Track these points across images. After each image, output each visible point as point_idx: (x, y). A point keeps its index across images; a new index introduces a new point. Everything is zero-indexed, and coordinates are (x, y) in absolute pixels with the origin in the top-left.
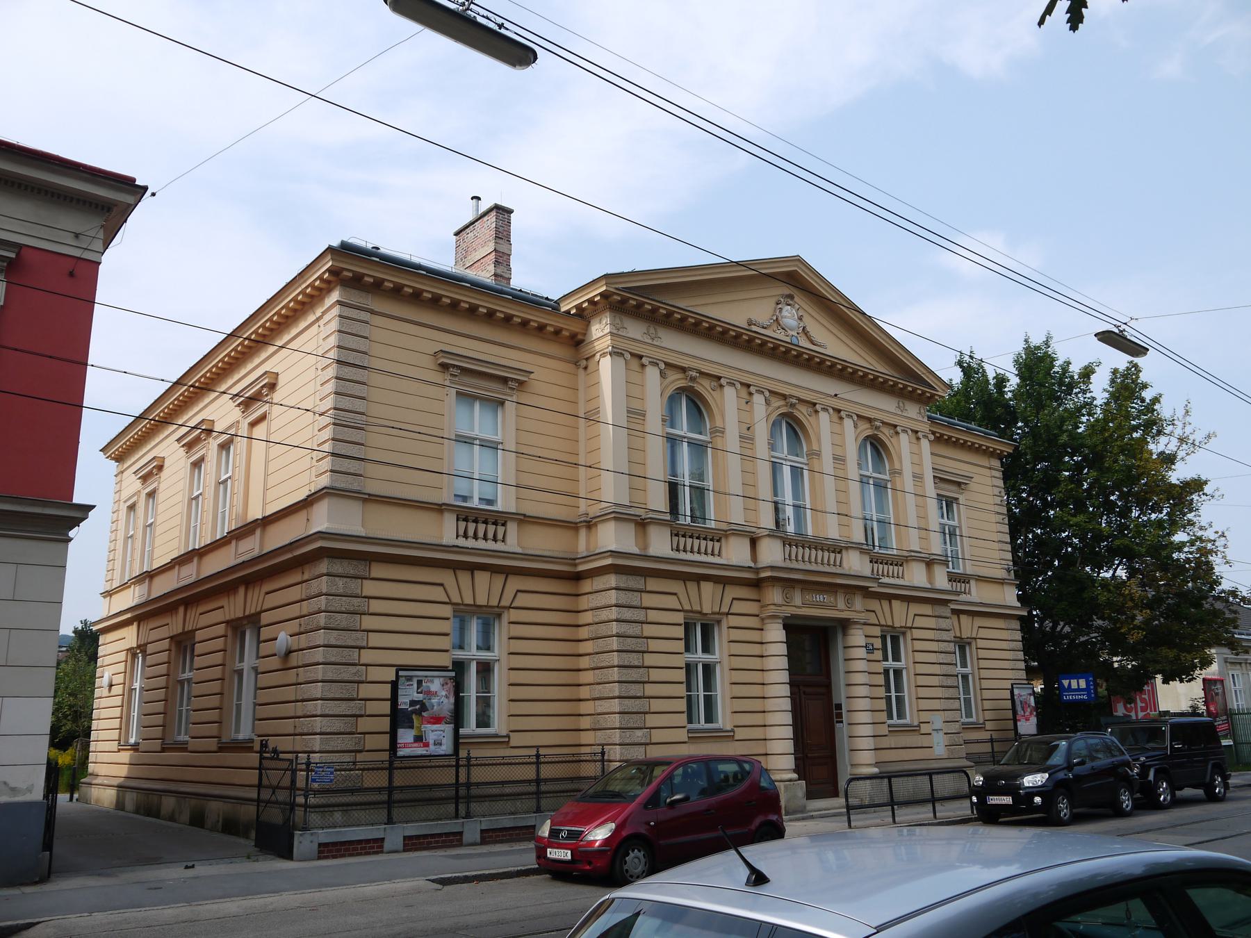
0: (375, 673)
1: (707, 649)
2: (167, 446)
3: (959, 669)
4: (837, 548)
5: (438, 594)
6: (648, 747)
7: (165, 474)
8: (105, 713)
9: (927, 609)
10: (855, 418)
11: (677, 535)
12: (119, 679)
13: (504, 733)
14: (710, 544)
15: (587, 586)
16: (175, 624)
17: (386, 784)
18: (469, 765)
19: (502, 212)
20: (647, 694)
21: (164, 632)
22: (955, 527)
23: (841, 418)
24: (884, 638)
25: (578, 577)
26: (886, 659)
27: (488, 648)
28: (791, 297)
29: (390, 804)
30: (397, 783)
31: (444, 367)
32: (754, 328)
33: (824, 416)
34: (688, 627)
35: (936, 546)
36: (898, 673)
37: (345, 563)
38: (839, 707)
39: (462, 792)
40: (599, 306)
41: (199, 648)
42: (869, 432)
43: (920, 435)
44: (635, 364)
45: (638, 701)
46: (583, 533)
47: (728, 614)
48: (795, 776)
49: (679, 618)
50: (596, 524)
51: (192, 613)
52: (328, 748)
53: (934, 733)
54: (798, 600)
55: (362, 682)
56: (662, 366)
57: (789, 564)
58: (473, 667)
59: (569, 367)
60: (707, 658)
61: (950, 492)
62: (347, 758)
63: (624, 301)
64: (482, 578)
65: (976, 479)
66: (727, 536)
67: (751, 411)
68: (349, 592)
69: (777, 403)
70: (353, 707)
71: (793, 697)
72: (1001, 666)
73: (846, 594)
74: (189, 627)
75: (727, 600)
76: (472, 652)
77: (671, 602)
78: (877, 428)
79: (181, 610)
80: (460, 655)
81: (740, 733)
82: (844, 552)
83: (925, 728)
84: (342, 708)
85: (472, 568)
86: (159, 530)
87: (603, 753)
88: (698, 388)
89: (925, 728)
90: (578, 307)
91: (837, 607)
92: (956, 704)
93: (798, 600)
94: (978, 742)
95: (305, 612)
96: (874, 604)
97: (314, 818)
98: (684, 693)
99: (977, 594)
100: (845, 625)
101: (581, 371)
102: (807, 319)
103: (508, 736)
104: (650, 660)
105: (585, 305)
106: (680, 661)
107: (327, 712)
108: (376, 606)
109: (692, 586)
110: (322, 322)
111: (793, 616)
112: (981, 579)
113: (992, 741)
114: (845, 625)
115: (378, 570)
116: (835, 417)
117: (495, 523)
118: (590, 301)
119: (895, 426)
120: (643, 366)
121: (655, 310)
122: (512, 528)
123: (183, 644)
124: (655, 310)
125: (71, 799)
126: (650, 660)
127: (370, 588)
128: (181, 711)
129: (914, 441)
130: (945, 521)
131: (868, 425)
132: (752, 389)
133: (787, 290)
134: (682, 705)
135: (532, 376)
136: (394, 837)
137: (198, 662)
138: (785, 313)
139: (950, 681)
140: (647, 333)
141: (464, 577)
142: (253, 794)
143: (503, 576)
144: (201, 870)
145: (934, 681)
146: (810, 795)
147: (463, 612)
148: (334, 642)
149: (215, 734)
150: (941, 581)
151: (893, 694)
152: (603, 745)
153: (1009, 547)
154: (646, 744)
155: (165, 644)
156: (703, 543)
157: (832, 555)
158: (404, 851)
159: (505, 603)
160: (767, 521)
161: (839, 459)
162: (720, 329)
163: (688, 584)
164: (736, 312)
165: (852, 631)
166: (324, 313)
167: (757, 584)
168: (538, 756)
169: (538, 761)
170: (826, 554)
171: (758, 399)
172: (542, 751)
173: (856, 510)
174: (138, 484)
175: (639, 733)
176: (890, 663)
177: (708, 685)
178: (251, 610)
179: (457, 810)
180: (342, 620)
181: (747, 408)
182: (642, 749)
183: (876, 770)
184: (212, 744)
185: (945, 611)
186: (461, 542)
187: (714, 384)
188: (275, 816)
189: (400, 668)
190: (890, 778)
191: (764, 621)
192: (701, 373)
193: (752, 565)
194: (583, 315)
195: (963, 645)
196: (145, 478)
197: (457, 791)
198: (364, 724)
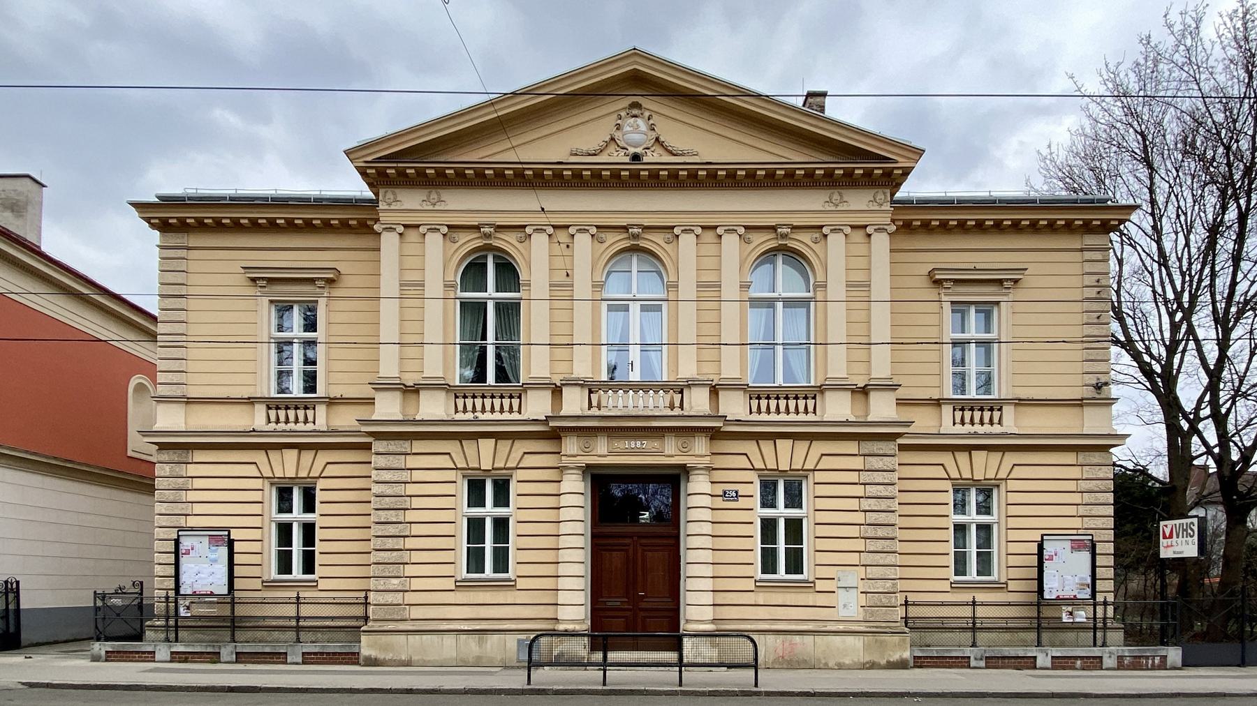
13: (1003, 581)
28: (636, 105)
31: (938, 283)
37: (171, 452)
44: (858, 236)
45: (395, 553)
53: (841, 592)
58: (974, 528)
66: (525, 391)
75: (516, 455)
87: (366, 598)
91: (668, 453)
115: (199, 456)
122: (1008, 411)
127: (192, 470)
159: (1002, 475)
167: (555, 435)
168: (298, 598)
189: (181, 529)
192: (794, 228)
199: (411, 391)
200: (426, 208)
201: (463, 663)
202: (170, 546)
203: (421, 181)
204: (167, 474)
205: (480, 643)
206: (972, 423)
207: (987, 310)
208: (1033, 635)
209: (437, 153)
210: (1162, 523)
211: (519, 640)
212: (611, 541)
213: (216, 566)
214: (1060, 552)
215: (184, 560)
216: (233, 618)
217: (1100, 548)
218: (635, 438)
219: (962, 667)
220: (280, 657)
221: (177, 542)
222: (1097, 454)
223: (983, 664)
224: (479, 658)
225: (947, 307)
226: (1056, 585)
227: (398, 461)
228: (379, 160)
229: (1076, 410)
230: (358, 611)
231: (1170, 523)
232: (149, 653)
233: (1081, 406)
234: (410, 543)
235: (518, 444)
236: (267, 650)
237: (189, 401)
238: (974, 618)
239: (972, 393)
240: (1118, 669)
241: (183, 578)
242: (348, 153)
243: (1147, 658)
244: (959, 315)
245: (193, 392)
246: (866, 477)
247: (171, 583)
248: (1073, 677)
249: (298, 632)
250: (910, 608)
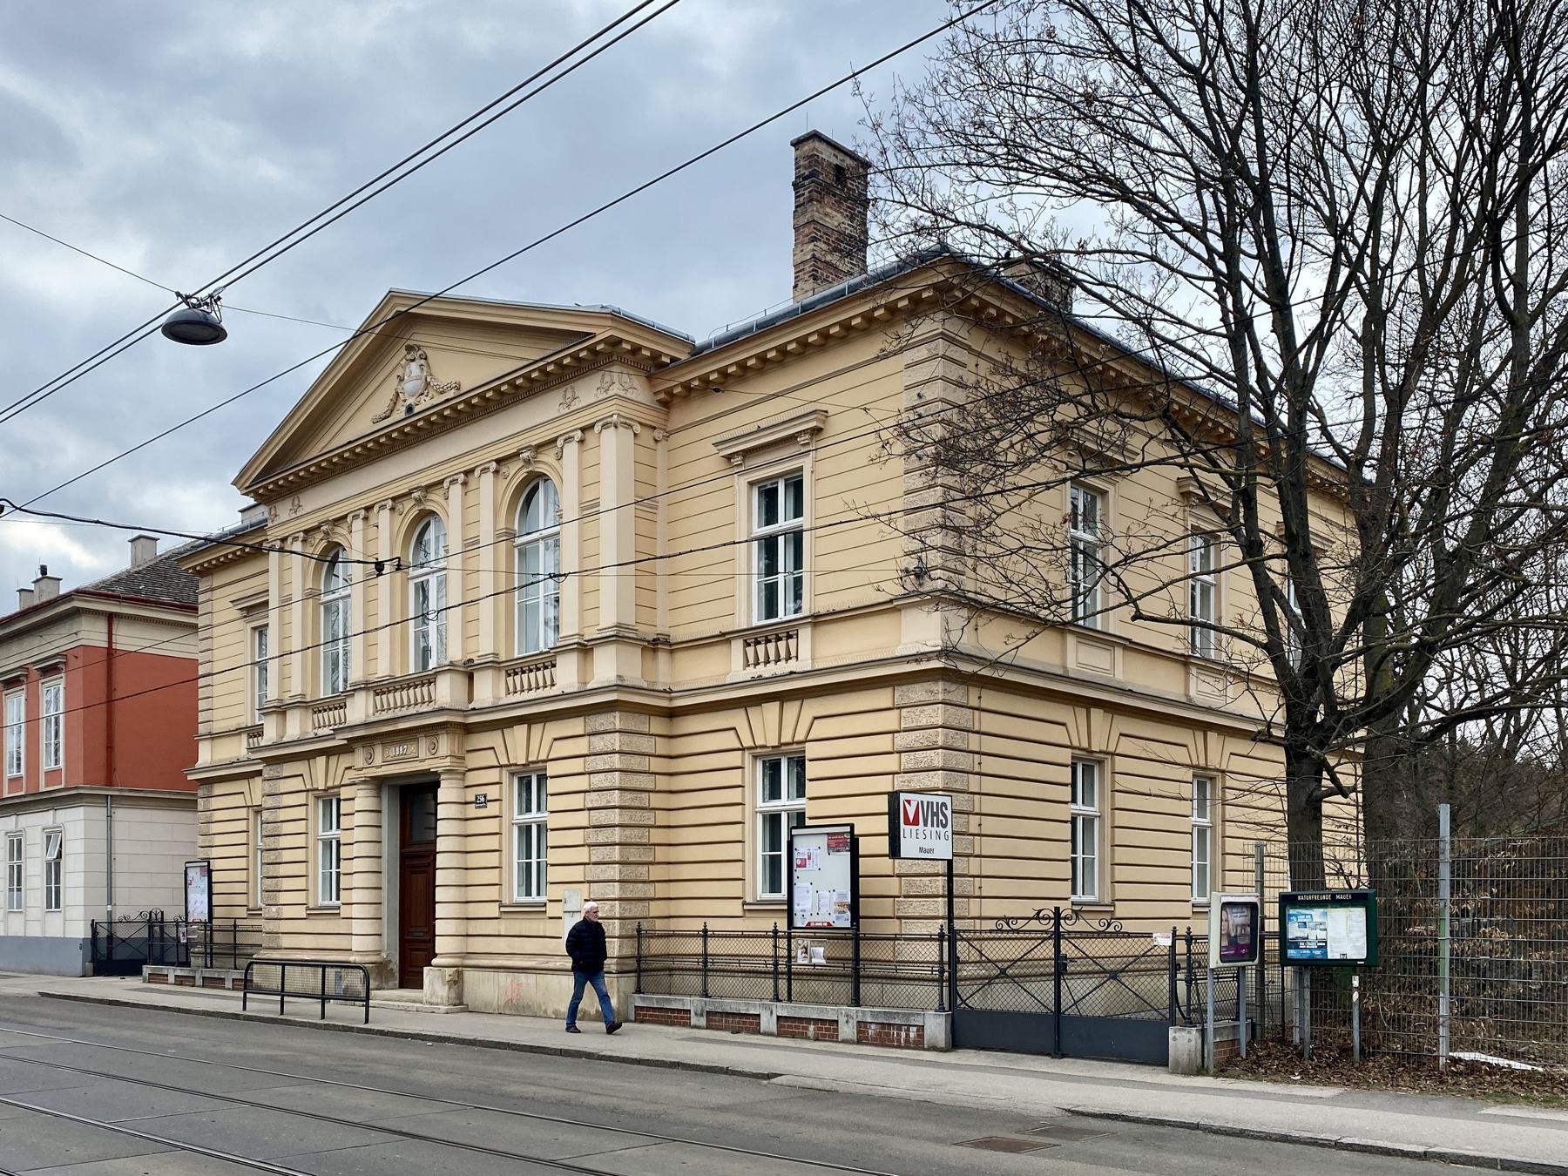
3: (1195, 819)
9: (576, 726)
26: (1074, 801)
49: (1065, 756)
106: (1065, 812)
115: (219, 789)
122: (805, 634)
168: (639, 931)
176: (1079, 808)
184: (301, 912)
208: (845, 988)
209: (294, 458)
212: (416, 862)
216: (235, 946)
217: (865, 846)
219: (679, 1024)
222: (918, 687)
223: (703, 1021)
226: (808, 906)
229: (721, 649)
238: (705, 955)
240: (859, 1042)
242: (234, 483)
243: (899, 1027)
248: (755, 1045)
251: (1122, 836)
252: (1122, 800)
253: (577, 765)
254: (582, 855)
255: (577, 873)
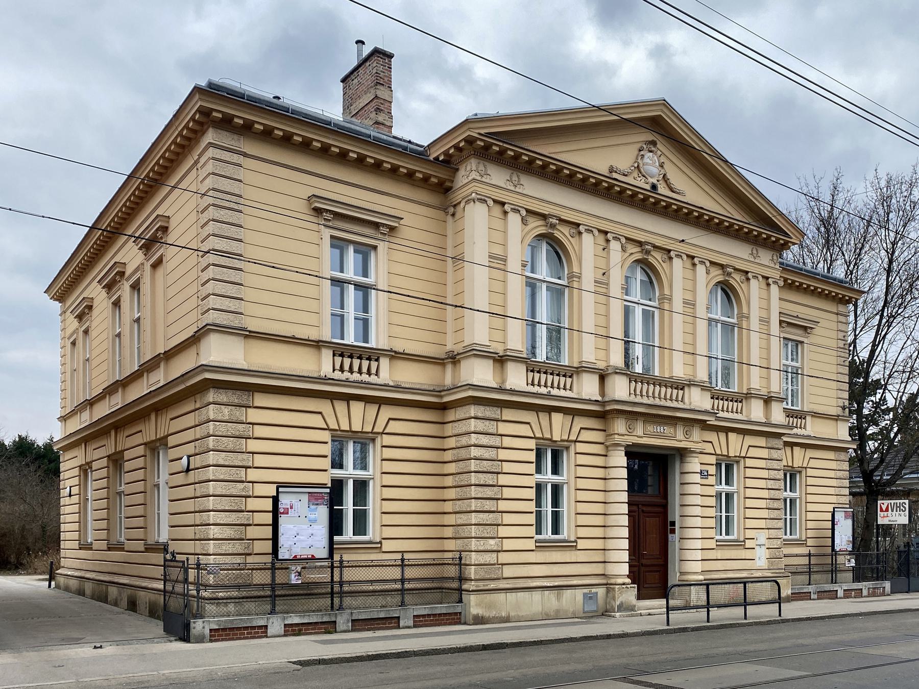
0: (260, 490)
1: (556, 471)
2: (92, 289)
4: (680, 386)
5: (317, 421)
6: (500, 554)
7: (95, 312)
8: (69, 518)
9: (761, 441)
10: (708, 264)
11: (532, 371)
12: (75, 490)
13: (573, 539)
14: (563, 379)
15: (451, 415)
16: (109, 446)
17: (399, 577)
18: (341, 567)
19: (381, 55)
20: (500, 509)
21: (103, 452)
22: (797, 368)
23: (506, 213)
24: (718, 465)
25: (444, 407)
27: (364, 468)
28: (654, 143)
29: (273, 598)
30: (278, 581)
31: (318, 211)
32: (615, 175)
33: (587, 238)
34: (539, 454)
35: (776, 384)
36: (729, 496)
37: (230, 392)
38: (673, 524)
39: (337, 588)
40: (465, 153)
41: (128, 466)
42: (721, 278)
43: (770, 281)
44: (497, 210)
45: (491, 515)
46: (449, 368)
47: (576, 441)
48: (628, 581)
49: (532, 444)
50: (459, 361)
51: (121, 436)
52: (220, 552)
53: (757, 548)
54: (639, 430)
55: (250, 497)
56: (524, 213)
57: (632, 398)
58: (350, 484)
59: (439, 214)
60: (556, 479)
61: (796, 335)
62: (238, 560)
63: (487, 147)
64: (357, 408)
65: (823, 323)
66: (578, 373)
67: (608, 258)
68: (234, 419)
69: (632, 249)
70: (242, 518)
71: (630, 514)
72: (827, 491)
73: (685, 426)
74: (119, 449)
75: (576, 429)
76: (350, 471)
77: (524, 430)
78: (553, 226)
79: (113, 433)
80: (338, 473)
81: (581, 544)
82: (686, 389)
83: (749, 544)
84: (233, 518)
85: (348, 398)
86: (94, 363)
87: (460, 558)
88: (557, 234)
89: (749, 544)
90: (446, 153)
91: (675, 438)
92: (780, 524)
93: (639, 430)
94: (797, 556)
95: (198, 436)
96: (712, 436)
97: (210, 608)
98: (534, 509)
99: (813, 428)
100: (682, 454)
101: (449, 218)
102: (668, 167)
103: (380, 543)
104: (503, 480)
105: (452, 151)
107: (218, 522)
108: (259, 431)
109: (544, 417)
110: (199, 165)
111: (635, 445)
112: (816, 415)
113: (810, 555)
114: (682, 454)
115: (260, 400)
116: (688, 263)
117: (369, 359)
118: (456, 147)
119: (747, 272)
120: (506, 213)
121: (517, 156)
122: (384, 362)
123: (116, 461)
124: (517, 156)
125: (50, 586)
126: (503, 480)
127: (254, 415)
128: (120, 518)
129: (690, 266)
130: (789, 362)
131: (720, 272)
132: (610, 236)
133: (650, 137)
134: (532, 519)
135: (402, 222)
136: (276, 625)
137: (127, 477)
138: (646, 160)
139: (776, 504)
140: (510, 180)
141: (341, 406)
142: (160, 586)
143: (377, 406)
144: (109, 650)
145: (762, 504)
146: (640, 597)
147: (339, 439)
148: (221, 462)
149: (105, 538)
150: (778, 415)
151: (788, 517)
152: (460, 551)
153: (846, 387)
154: (498, 551)
155: (104, 462)
156: (556, 378)
157: (675, 391)
158: (285, 635)
160: (617, 359)
161: (690, 304)
162: (618, 189)
163: (540, 414)
164: (596, 158)
165: (689, 459)
166: (200, 155)
168: (403, 560)
169: (403, 565)
170: (669, 390)
171: (615, 246)
172: (406, 556)
173: (702, 348)
174: (76, 323)
175: (492, 542)
177: (556, 502)
178: (161, 434)
179: (332, 603)
180: (230, 443)
181: (604, 254)
182: (494, 555)
183: (701, 577)
184: (140, 546)
185: (778, 443)
186: (338, 375)
187: (573, 231)
188: (175, 604)
189: (280, 485)
190: (745, 583)
191: (608, 447)
192: (561, 220)
193: (600, 399)
194: (449, 163)
195: (792, 475)
196: (80, 317)
197: (332, 589)
198: (252, 532)
199: (501, 360)
200: (509, 187)
201: (547, 617)
202: (268, 504)
203: (500, 159)
204: (226, 418)
205: (559, 598)
206: (360, 372)
207: (365, 251)
210: (879, 502)
211: (585, 594)
213: (315, 526)
214: (297, 505)
215: (282, 519)
218: (660, 424)
220: (392, 622)
221: (276, 500)
224: (558, 611)
225: (327, 241)
227: (490, 427)
228: (489, 135)
229: (832, 423)
230: (452, 571)
231: (886, 502)
232: (260, 627)
233: (837, 420)
234: (503, 505)
235: (577, 419)
236: (382, 615)
237: (250, 335)
239: (350, 339)
241: (282, 540)
244: (337, 251)
245: (253, 325)
246: (496, 441)
247: (268, 546)
249: (403, 595)
250: (407, 569)
251: (810, 507)
252: (810, 490)
253: (762, 464)
254: (765, 514)
255: (762, 523)
